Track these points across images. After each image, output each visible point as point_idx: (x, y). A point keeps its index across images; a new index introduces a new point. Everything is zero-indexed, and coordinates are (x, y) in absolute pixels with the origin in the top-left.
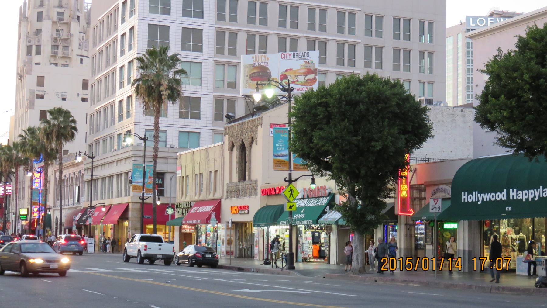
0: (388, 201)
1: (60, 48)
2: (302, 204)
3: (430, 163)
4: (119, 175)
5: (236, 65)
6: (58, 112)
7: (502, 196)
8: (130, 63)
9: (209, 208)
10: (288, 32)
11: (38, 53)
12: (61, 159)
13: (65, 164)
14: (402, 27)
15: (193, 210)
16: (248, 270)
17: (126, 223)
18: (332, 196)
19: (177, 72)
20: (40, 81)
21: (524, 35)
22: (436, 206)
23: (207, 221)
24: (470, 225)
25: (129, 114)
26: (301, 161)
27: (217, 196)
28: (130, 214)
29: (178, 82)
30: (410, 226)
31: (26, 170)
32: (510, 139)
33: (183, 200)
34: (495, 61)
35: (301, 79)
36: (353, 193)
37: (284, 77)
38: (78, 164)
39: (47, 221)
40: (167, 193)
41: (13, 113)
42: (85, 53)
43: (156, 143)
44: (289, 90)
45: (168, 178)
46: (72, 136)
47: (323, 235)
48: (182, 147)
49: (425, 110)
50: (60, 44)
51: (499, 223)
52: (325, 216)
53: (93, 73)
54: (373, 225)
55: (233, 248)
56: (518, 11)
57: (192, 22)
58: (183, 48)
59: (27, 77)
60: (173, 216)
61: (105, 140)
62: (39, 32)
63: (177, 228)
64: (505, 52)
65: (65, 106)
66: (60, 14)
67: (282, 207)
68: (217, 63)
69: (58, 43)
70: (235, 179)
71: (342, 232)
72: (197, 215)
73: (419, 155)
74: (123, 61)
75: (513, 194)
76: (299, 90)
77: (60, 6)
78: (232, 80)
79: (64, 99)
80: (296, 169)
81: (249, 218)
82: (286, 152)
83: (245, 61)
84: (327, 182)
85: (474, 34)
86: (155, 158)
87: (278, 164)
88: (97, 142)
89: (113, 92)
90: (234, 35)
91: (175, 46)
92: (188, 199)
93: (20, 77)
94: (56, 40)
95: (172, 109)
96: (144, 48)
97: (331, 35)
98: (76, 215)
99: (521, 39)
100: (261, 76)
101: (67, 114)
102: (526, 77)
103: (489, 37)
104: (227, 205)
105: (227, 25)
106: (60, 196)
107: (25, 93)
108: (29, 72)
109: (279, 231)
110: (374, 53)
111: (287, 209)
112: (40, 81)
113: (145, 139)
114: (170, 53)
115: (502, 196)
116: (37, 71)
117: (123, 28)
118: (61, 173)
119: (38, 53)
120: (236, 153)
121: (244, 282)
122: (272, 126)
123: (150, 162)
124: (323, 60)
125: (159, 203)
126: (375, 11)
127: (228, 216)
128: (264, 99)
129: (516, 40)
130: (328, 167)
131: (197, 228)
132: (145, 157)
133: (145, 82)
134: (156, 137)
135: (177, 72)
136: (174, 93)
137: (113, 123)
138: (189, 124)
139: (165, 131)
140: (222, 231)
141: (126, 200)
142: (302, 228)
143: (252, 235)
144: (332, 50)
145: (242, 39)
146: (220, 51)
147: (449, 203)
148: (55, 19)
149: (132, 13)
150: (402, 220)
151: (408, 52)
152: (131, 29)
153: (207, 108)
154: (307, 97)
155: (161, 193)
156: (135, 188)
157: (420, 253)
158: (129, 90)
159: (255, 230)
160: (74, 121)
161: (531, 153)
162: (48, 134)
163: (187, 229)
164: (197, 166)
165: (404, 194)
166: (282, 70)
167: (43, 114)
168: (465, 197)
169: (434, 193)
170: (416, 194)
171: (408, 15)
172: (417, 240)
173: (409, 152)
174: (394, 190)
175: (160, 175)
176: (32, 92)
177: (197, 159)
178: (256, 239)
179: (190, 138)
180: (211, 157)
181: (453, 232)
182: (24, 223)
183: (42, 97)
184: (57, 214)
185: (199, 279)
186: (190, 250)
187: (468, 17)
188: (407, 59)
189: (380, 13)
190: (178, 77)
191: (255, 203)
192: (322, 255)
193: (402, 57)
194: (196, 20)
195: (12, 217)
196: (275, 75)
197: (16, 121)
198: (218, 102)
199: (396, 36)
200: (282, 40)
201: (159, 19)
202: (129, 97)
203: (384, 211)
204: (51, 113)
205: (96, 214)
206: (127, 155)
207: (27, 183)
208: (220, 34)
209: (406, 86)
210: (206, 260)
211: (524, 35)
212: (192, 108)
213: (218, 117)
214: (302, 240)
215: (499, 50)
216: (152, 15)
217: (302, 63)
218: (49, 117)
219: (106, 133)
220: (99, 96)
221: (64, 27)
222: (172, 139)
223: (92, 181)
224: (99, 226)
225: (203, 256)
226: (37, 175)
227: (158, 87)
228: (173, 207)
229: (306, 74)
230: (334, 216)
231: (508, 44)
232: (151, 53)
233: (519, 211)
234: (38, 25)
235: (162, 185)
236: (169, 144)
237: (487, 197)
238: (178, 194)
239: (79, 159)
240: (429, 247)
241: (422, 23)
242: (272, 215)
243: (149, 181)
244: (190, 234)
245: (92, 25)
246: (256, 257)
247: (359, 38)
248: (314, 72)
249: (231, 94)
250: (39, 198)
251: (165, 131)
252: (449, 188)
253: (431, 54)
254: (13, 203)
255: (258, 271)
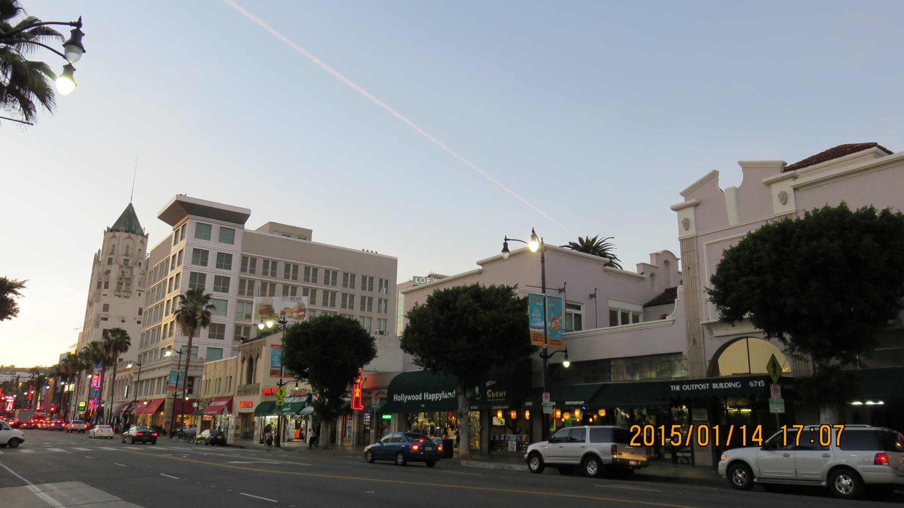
0: (346, 399)
1: (124, 285)
2: (289, 400)
3: (378, 375)
4: (160, 378)
5: (252, 303)
6: (116, 331)
7: (418, 397)
8: (174, 298)
9: (224, 403)
10: (290, 282)
11: (106, 287)
12: (116, 365)
13: (118, 369)
14: (367, 283)
15: (212, 404)
16: (248, 448)
17: (162, 413)
18: (310, 396)
19: (208, 307)
20: (106, 308)
21: (432, 295)
22: (376, 403)
23: (221, 413)
24: (399, 417)
25: (171, 334)
26: (288, 371)
27: (231, 394)
28: (166, 407)
29: (208, 314)
30: (361, 416)
31: (88, 373)
32: (422, 361)
33: (206, 396)
34: (414, 310)
35: (295, 315)
36: (322, 393)
37: (283, 313)
38: (129, 369)
39: (100, 412)
40: (195, 392)
41: (81, 330)
42: (142, 289)
43: (189, 356)
44: (284, 323)
45: (196, 381)
46: (126, 349)
47: (303, 422)
48: (208, 359)
49: (373, 339)
50: (124, 283)
51: (417, 415)
52: (305, 410)
53: (147, 304)
54: (336, 416)
55: (239, 432)
56: (446, 275)
57: (223, 272)
58: (215, 289)
59: (95, 304)
60: (198, 408)
61: (151, 352)
62: (108, 272)
63: (200, 417)
64: (420, 305)
65: (123, 327)
66: (126, 260)
67: (274, 402)
68: (239, 301)
69: (123, 281)
70: (244, 382)
71: (315, 420)
72: (214, 408)
73: (368, 369)
74: (169, 296)
75: (426, 396)
76: (291, 322)
77: (127, 255)
78: (249, 312)
79: (123, 321)
80: (286, 376)
81: (252, 410)
82: (279, 365)
83: (257, 300)
84: (305, 386)
85: (413, 288)
86: (187, 366)
87: (273, 373)
88: (145, 354)
89: (161, 318)
90: (252, 282)
91: (209, 288)
92: (209, 396)
93: (90, 304)
94: (121, 278)
95: (204, 332)
96: (187, 288)
97: (320, 286)
98: (124, 407)
99: (429, 297)
100: (267, 312)
101: (124, 333)
102: (431, 321)
103: (415, 293)
104: (237, 401)
105: (248, 276)
106: (112, 393)
107: (93, 316)
108: (98, 301)
109: (271, 419)
110: (348, 300)
111: (278, 404)
112: (106, 308)
113: (181, 353)
114: (204, 294)
115: (418, 397)
116: (104, 300)
117: (172, 274)
118: (115, 375)
119: (106, 287)
120: (246, 364)
121: (238, 456)
122: (272, 346)
123: (183, 369)
124: (313, 302)
125: (187, 399)
126: (350, 271)
127: (238, 408)
128: (266, 327)
129: (427, 298)
130: (306, 376)
131: (214, 418)
132: (179, 365)
133: (184, 313)
134: (189, 352)
135: (208, 307)
136: (206, 322)
137: (158, 340)
138: (216, 343)
139: (197, 347)
140: (232, 419)
141: (164, 396)
142: (289, 417)
143: (254, 423)
144: (319, 296)
145: (257, 285)
146: (241, 293)
147: (385, 402)
148: (122, 263)
149: (179, 264)
150: (356, 413)
151: (371, 299)
152: (178, 275)
153: (229, 332)
154: (296, 327)
155: (190, 392)
156: (171, 388)
157: (367, 435)
158: (171, 317)
159: (256, 419)
160: (128, 338)
161: (435, 370)
162: (107, 347)
163: (207, 418)
164: (228, 371)
165: (357, 395)
166: (282, 308)
167: (105, 332)
168: (396, 398)
169: (377, 395)
170: (365, 395)
171: (371, 275)
172: (365, 426)
173: (362, 366)
174: (350, 392)
175: (192, 379)
176: (98, 315)
177: (218, 367)
178: (256, 425)
179: (215, 353)
180: (228, 367)
181: (388, 421)
182: (81, 413)
183: (106, 319)
184: (109, 406)
185: (206, 454)
186: (206, 434)
187: (414, 277)
188: (370, 303)
189: (353, 272)
190: (209, 310)
191: (257, 400)
192: (302, 437)
193: (367, 303)
194: (226, 271)
195: (73, 408)
196: (277, 311)
197: (83, 336)
198: (238, 328)
199: (364, 288)
200: (286, 287)
201: (199, 269)
202: (172, 323)
203: (343, 407)
204: (111, 331)
205: (139, 406)
206: (167, 363)
207: (87, 383)
208: (242, 281)
209: (361, 324)
210: (218, 441)
211: (432, 295)
212: (218, 332)
213: (237, 338)
214: (288, 426)
215: (416, 303)
216: (194, 266)
217: (296, 304)
218: (110, 334)
219: (154, 346)
220: (149, 320)
221: (129, 271)
222: (202, 353)
223: (139, 382)
224: (141, 416)
225: (423, 450)
226: (96, 377)
227: (194, 314)
228: (198, 402)
229: (298, 312)
230: (310, 409)
231: (422, 300)
232: (189, 293)
233: (431, 408)
234: (108, 268)
235: (192, 386)
236: (199, 356)
237: (410, 398)
238: (205, 391)
239: (130, 366)
240: (372, 431)
241: (381, 280)
242: (267, 408)
243: (181, 383)
244: (209, 422)
245: (149, 270)
246: (255, 438)
247: (339, 288)
248: (304, 310)
249: (247, 323)
250: (96, 395)
251: (197, 347)
252: (386, 391)
253: (386, 301)
254: (74, 398)
255: (257, 448)
